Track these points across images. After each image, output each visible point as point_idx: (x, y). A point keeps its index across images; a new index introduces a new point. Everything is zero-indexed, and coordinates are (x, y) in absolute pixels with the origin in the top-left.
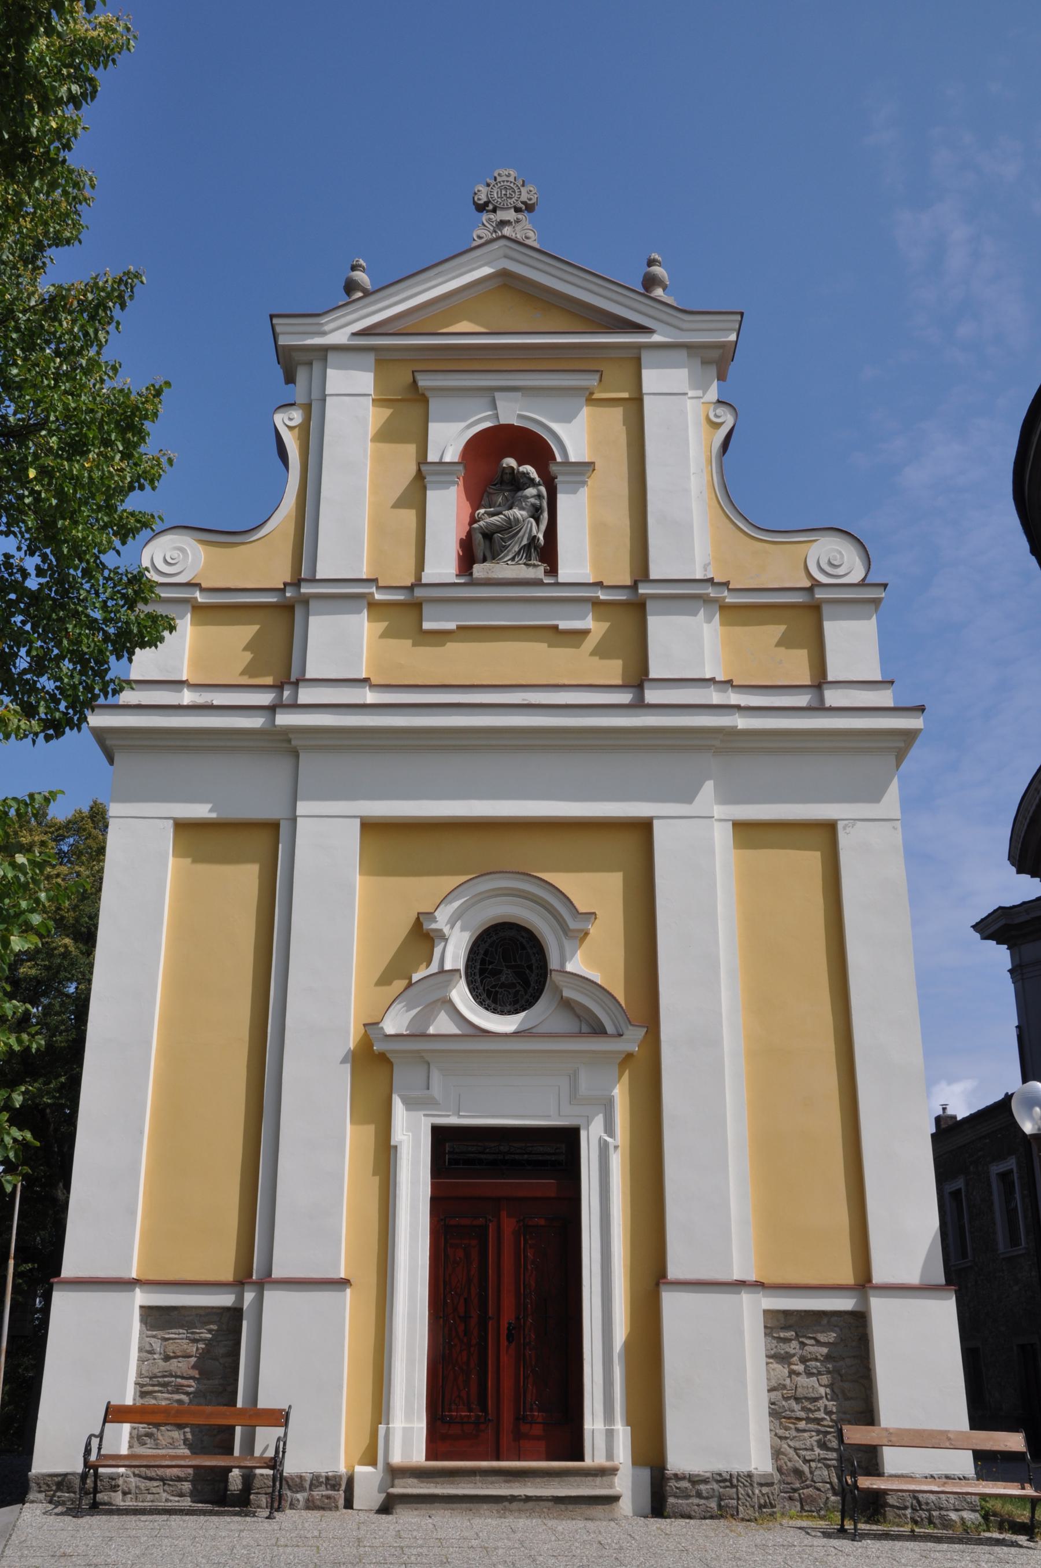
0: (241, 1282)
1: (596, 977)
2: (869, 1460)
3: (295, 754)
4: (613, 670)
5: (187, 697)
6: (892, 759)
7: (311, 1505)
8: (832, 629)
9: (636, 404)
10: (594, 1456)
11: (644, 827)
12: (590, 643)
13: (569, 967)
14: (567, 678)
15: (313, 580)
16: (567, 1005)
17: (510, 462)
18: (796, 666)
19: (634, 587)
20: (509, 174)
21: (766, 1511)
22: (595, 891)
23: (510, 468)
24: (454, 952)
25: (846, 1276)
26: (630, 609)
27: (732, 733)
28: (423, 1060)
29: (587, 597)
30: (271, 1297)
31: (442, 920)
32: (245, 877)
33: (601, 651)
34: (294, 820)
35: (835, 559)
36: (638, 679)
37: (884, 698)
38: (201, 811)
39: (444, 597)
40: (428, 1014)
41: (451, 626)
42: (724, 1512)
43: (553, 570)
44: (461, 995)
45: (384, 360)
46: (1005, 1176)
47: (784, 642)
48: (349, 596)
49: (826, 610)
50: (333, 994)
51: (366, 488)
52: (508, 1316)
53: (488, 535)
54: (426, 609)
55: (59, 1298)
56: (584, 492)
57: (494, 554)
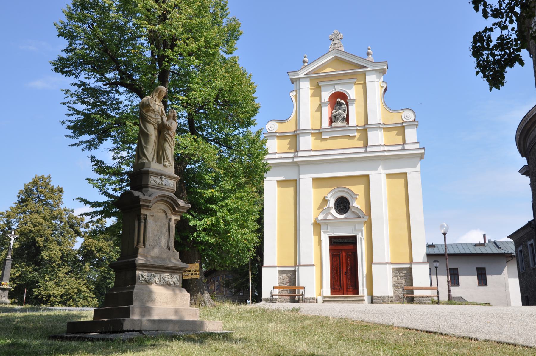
0: (295, 266)
1: (359, 207)
2: (412, 292)
3: (299, 166)
4: (361, 144)
5: (277, 156)
6: (419, 159)
7: (310, 302)
8: (407, 131)
9: (365, 84)
10: (360, 293)
11: (368, 176)
12: (356, 138)
13: (354, 205)
14: (350, 147)
15: (300, 130)
16: (353, 212)
17: (339, 100)
19: (365, 126)
21: (392, 302)
22: (358, 189)
23: (339, 100)
24: (332, 203)
25: (408, 261)
26: (364, 131)
27: (385, 156)
28: (326, 224)
29: (355, 129)
30: (300, 267)
31: (328, 197)
32: (291, 190)
33: (359, 139)
34: (299, 179)
35: (409, 116)
36: (366, 146)
37: (417, 146)
38: (282, 178)
39: (326, 131)
41: (328, 137)
43: (348, 123)
44: (333, 211)
45: (311, 79)
46: (531, 245)
47: (397, 135)
48: (307, 133)
49: (405, 127)
50: (309, 211)
51: (310, 108)
52: (344, 270)
53: (335, 117)
57: (336, 121)
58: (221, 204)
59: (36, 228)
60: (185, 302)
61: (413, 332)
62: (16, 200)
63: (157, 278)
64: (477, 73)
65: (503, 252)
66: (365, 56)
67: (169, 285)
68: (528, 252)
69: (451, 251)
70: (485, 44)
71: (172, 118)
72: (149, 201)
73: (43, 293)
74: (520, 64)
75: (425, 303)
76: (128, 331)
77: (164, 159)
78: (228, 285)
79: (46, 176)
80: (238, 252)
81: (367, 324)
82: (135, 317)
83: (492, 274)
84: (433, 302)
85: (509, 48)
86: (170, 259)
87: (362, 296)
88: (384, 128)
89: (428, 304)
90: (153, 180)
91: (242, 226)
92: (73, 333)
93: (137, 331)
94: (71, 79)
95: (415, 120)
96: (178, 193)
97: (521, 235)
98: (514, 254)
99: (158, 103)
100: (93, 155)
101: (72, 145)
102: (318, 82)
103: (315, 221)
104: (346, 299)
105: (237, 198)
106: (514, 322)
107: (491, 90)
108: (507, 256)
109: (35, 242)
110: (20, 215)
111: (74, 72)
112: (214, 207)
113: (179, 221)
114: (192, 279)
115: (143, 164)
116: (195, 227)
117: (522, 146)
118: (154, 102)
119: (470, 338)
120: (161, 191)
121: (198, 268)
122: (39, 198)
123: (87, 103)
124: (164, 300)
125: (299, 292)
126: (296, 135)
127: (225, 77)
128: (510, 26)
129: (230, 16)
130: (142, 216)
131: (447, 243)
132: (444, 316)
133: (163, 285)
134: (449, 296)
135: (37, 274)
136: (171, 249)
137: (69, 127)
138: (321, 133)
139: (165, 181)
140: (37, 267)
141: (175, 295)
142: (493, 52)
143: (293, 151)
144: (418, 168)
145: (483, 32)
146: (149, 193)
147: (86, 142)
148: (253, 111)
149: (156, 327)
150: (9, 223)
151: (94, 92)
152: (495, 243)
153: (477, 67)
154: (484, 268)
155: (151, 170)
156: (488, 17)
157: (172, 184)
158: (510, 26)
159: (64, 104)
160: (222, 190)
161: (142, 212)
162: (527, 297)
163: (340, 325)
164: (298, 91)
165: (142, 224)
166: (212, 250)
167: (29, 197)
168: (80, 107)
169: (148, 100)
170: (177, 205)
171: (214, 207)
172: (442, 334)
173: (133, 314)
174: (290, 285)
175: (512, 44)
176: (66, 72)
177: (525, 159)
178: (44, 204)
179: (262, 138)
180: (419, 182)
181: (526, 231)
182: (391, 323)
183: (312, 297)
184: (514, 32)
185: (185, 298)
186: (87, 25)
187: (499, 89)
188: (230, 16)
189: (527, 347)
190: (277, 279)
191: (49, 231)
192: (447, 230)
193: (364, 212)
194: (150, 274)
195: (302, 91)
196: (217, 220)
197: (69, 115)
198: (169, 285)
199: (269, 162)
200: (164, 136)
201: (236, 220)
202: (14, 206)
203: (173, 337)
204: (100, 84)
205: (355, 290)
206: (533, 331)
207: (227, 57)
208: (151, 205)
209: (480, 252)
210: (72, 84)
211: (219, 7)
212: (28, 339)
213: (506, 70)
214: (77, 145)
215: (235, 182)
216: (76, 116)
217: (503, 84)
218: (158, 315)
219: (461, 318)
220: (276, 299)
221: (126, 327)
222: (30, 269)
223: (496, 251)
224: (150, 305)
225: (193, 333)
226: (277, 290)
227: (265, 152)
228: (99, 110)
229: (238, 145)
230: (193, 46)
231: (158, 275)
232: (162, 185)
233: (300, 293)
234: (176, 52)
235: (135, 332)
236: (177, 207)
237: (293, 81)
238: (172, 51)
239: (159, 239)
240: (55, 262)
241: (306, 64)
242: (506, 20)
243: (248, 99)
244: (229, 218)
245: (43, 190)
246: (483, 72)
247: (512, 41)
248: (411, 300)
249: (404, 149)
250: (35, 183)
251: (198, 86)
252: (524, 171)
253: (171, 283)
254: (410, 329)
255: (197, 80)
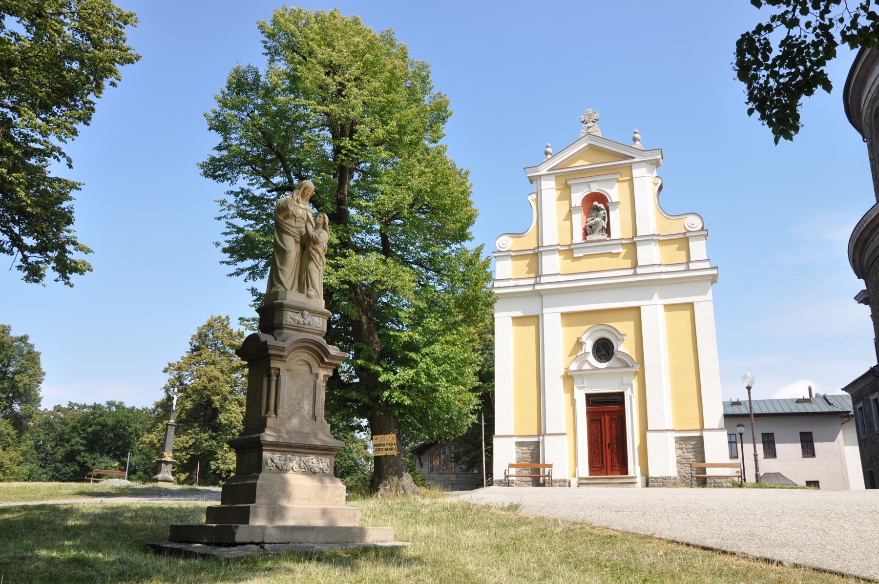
0: (539, 434)
2: (704, 471)
4: (628, 263)
5: (512, 283)
7: (560, 486)
8: (692, 244)
9: (631, 180)
10: (631, 473)
12: (621, 256)
13: (620, 349)
14: (615, 268)
15: (542, 246)
16: (619, 359)
17: (596, 203)
18: (682, 256)
20: (590, 110)
21: (675, 485)
22: (625, 327)
23: (596, 204)
24: (589, 347)
26: (632, 245)
28: (582, 377)
29: (620, 243)
31: (584, 339)
33: (625, 258)
35: (694, 223)
36: (635, 266)
37: (707, 265)
38: (519, 314)
39: (579, 247)
40: (582, 364)
41: (581, 255)
42: (664, 485)
43: (609, 236)
44: (591, 358)
45: (557, 176)
47: (678, 249)
48: (552, 250)
51: (556, 217)
52: (608, 441)
53: (591, 227)
54: (574, 251)
55: (495, 439)
56: (617, 210)
57: (592, 232)
58: (424, 351)
59: (212, 384)
60: (337, 499)
61: (680, 548)
62: (188, 348)
63: (294, 462)
64: (750, 112)
65: (836, 410)
66: (631, 143)
67: (314, 473)
68: (870, 410)
69: (756, 410)
70: (760, 57)
71: (321, 226)
72: (283, 349)
73: (222, 467)
74: (824, 88)
75: (723, 487)
76: (243, 544)
77: (308, 286)
78: (457, 459)
79: (223, 317)
80: (451, 418)
81: (612, 533)
82: (258, 521)
83: (821, 441)
84: (735, 485)
85: (803, 63)
86: (315, 435)
87: (632, 477)
88: (659, 241)
89: (727, 487)
90: (290, 318)
91: (455, 382)
92: (181, 542)
93: (257, 544)
94: (226, 186)
95: (702, 228)
96: (332, 336)
97: (861, 385)
98: (852, 413)
99: (302, 205)
100: (255, 287)
101: (231, 275)
102: (566, 180)
103: (566, 373)
104: (611, 481)
105: (447, 342)
106: (846, 526)
107: (776, 141)
108: (841, 416)
109: (210, 402)
110: (193, 366)
111: (229, 176)
112: (413, 355)
113: (330, 378)
114: (386, 456)
115: (277, 293)
116: (387, 385)
117: (858, 262)
118: (296, 203)
119: (768, 561)
120: (304, 334)
121: (395, 441)
122: (216, 345)
123: (250, 217)
124: (307, 496)
125: (544, 472)
126: (537, 254)
127: (424, 173)
128: (803, 20)
129: (434, 91)
130: (272, 371)
131: (752, 399)
132: (738, 514)
133: (304, 473)
134: (757, 476)
135: (215, 442)
136: (318, 418)
137: (225, 250)
138: (572, 250)
139: (309, 318)
140: (214, 434)
141: (324, 488)
142: (777, 69)
143: (533, 275)
144: (710, 295)
145: (754, 32)
146: (283, 337)
147: (249, 269)
148: (467, 219)
149: (286, 537)
150: (180, 377)
151: (256, 201)
152: (825, 397)
153: (750, 99)
154: (811, 433)
155: (285, 302)
156: (761, 4)
157: (320, 324)
158: (803, 20)
159: (219, 219)
160: (426, 331)
161: (272, 365)
162: (871, 472)
163: (571, 534)
164: (538, 193)
165: (273, 383)
166: (413, 415)
167: (204, 343)
168: (240, 223)
169: (286, 202)
170: (327, 353)
171: (413, 355)
172: (725, 552)
173: (255, 516)
174: (532, 462)
175: (808, 53)
176: (219, 176)
177: (862, 281)
178: (222, 353)
179: (482, 258)
180: (711, 315)
181: (867, 381)
182: (649, 533)
183: (562, 478)
184: (811, 30)
185: (338, 492)
186: (245, 113)
187: (791, 140)
188: (434, 91)
189: (864, 579)
190: (514, 454)
191: (227, 388)
192: (753, 381)
193: (634, 359)
194: (283, 457)
195: (544, 194)
196: (417, 374)
197: (226, 234)
198: (314, 473)
199: (497, 291)
200: (309, 252)
201: (444, 373)
202: (186, 355)
203: (306, 555)
204: (264, 190)
205: (623, 468)
206: (876, 541)
207: (432, 146)
208: (285, 354)
209: (804, 411)
210: (228, 193)
211: (419, 79)
212: (104, 554)
213: (800, 101)
214: (238, 274)
215: (444, 320)
216: (235, 235)
217: (797, 129)
218: (294, 518)
219: (764, 519)
220: (513, 482)
221: (239, 538)
222: (206, 436)
223: (826, 408)
224: (284, 503)
225: (342, 547)
226: (514, 469)
227: (489, 278)
228: (265, 225)
229: (452, 269)
230: (380, 133)
231: (297, 458)
232: (304, 324)
233: (546, 473)
234: (356, 141)
235: (253, 546)
236: (327, 357)
237: (531, 180)
238: (351, 139)
239: (299, 404)
240: (235, 428)
241: (549, 156)
242: (794, 10)
243: (461, 201)
244: (434, 371)
245: (220, 334)
246: (761, 109)
247: (807, 47)
248: (703, 482)
249: (688, 270)
250: (210, 325)
251: (387, 186)
252: (863, 298)
253: (317, 470)
254: (678, 543)
255: (385, 179)
